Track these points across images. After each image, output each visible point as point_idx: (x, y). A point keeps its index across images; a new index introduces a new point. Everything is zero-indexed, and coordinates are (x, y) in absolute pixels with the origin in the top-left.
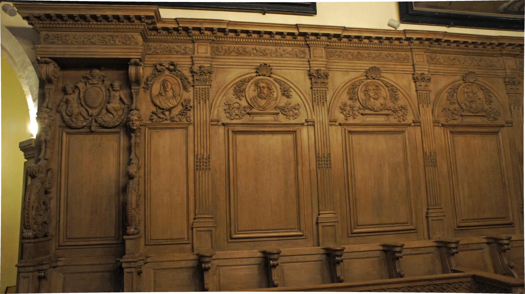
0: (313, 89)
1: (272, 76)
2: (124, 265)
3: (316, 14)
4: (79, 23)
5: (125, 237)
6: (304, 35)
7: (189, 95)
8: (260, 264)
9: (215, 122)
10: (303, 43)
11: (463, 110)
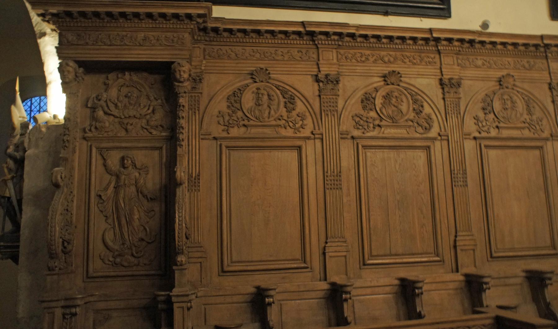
0: (322, 97)
1: (402, 84)
2: (174, 299)
3: (450, 17)
4: (143, 21)
5: (174, 268)
6: (437, 40)
8: (396, 293)
9: (343, 136)
10: (434, 48)
11: (249, 119)
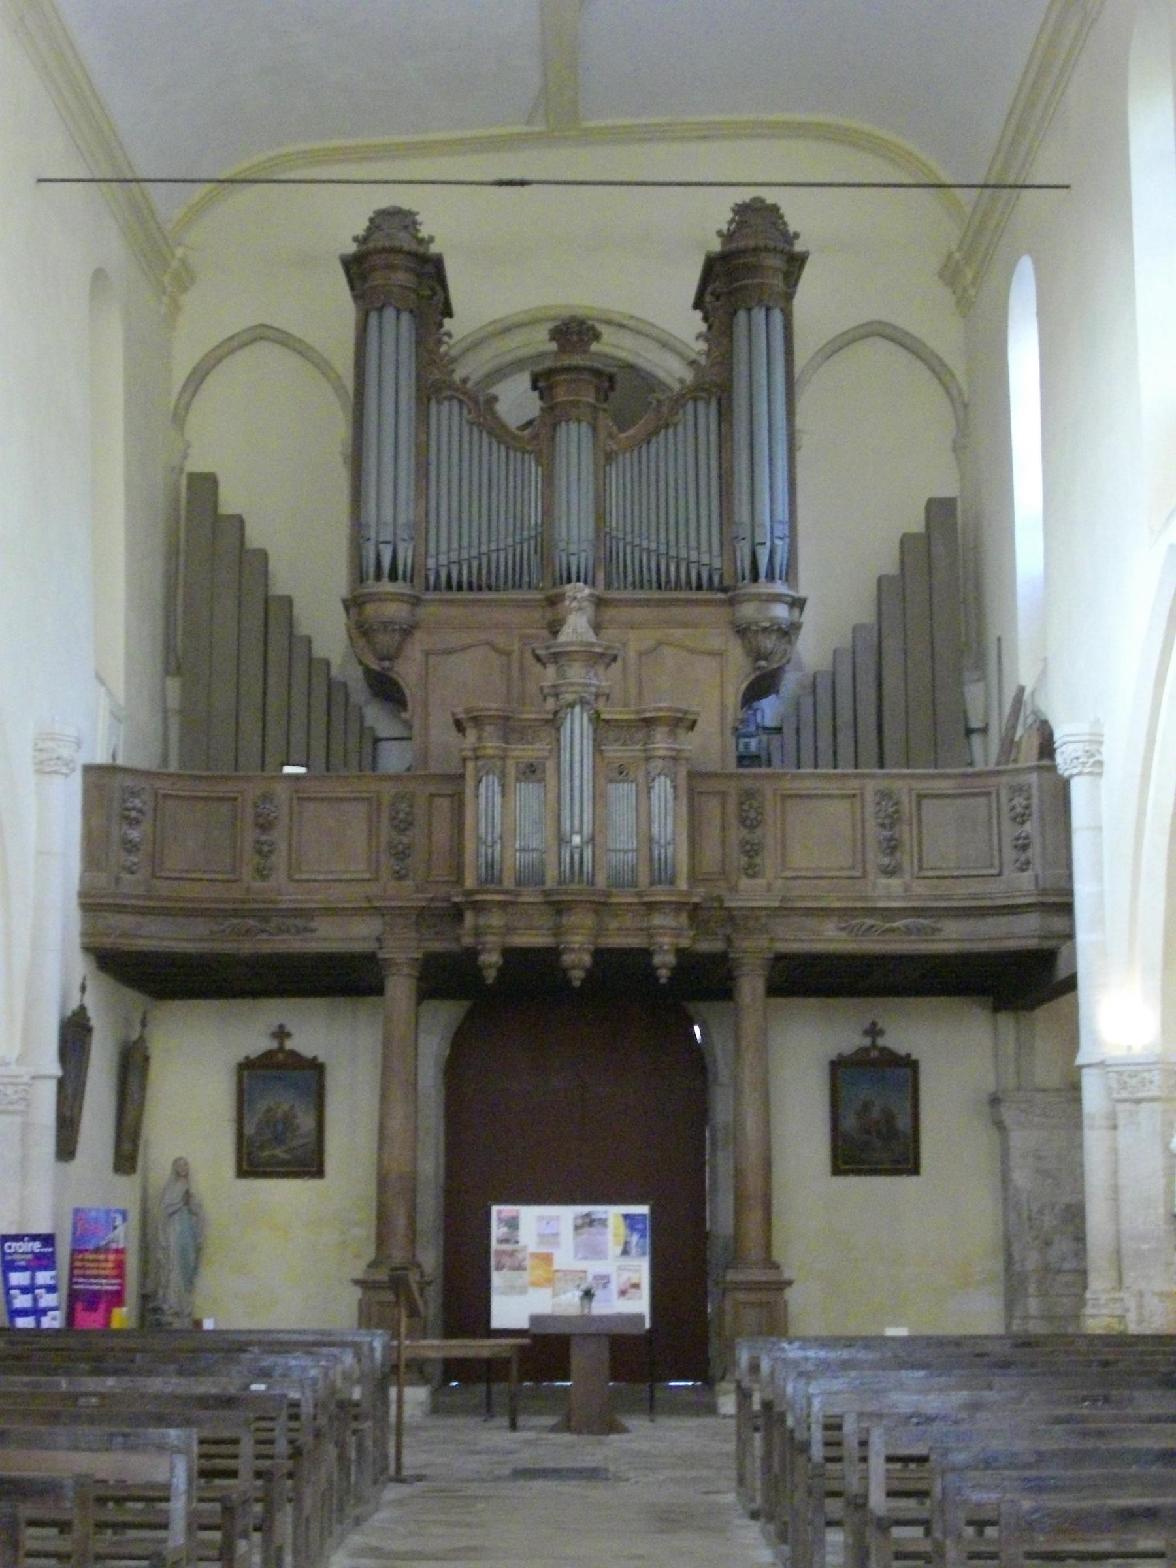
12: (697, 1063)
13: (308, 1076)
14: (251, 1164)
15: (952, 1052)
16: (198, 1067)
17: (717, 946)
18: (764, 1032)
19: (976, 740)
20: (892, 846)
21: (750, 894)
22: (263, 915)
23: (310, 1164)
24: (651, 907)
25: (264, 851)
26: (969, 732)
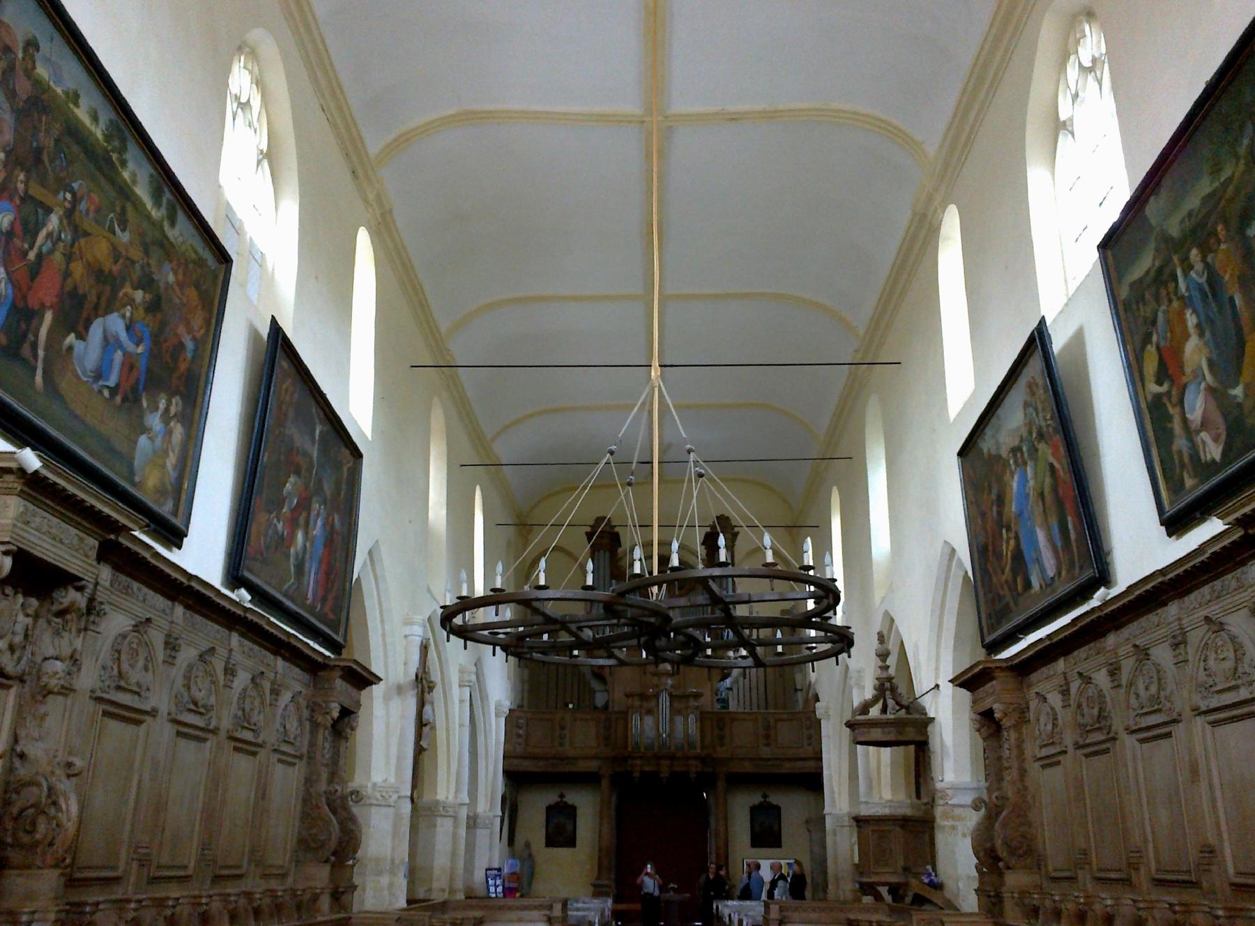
3: (180, 547)
7: (78, 643)
12: (704, 808)
13: (571, 812)
14: (550, 842)
15: (792, 807)
16: (536, 806)
17: (710, 770)
18: (725, 800)
19: (799, 694)
20: (767, 737)
21: (721, 752)
22: (562, 759)
23: (571, 842)
24: (689, 758)
25: (562, 737)
26: (796, 690)
